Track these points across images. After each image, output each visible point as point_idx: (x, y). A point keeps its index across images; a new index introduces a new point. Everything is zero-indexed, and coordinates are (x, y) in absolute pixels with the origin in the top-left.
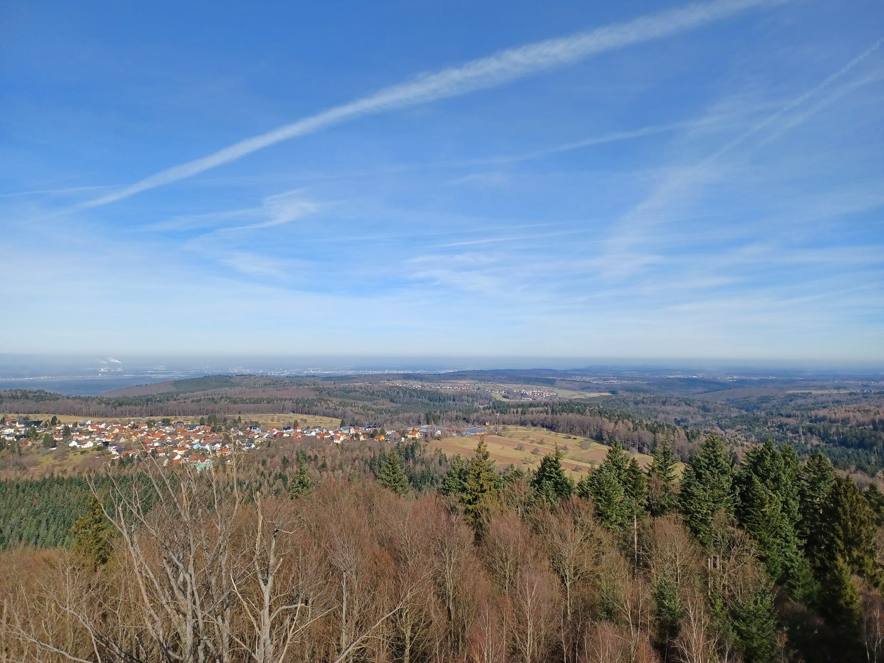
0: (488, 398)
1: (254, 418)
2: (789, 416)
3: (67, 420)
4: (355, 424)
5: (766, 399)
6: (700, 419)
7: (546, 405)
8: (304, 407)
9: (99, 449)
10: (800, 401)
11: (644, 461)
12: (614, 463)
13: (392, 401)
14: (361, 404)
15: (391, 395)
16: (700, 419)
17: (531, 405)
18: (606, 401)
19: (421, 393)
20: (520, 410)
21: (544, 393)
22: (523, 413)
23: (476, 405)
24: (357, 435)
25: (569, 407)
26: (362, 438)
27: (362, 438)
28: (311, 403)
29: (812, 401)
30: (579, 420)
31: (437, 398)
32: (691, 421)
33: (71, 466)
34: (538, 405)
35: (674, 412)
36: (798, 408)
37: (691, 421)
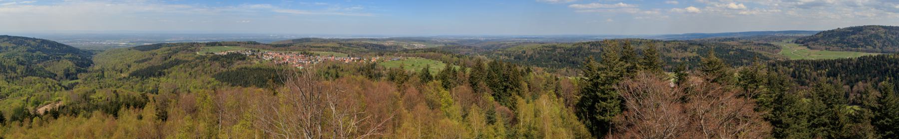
0: (401, 47)
1: (318, 52)
2: (499, 51)
3: (262, 51)
4: (353, 56)
5: (493, 46)
6: (473, 53)
7: (422, 49)
8: (335, 49)
9: (271, 60)
10: (503, 46)
11: (457, 68)
12: (449, 69)
13: (366, 48)
14: (355, 49)
15: (366, 46)
16: (473, 53)
17: (417, 50)
18: (443, 48)
19: (377, 45)
20: (413, 51)
21: (421, 46)
22: (414, 52)
23: (397, 50)
24: (354, 60)
25: (431, 50)
26: (355, 61)
27: (355, 61)
28: (337, 48)
29: (505, 45)
30: (572, 68)
31: (384, 47)
32: (471, 54)
33: (265, 65)
34: (420, 49)
35: (466, 51)
36: (502, 48)
37: (471, 54)
